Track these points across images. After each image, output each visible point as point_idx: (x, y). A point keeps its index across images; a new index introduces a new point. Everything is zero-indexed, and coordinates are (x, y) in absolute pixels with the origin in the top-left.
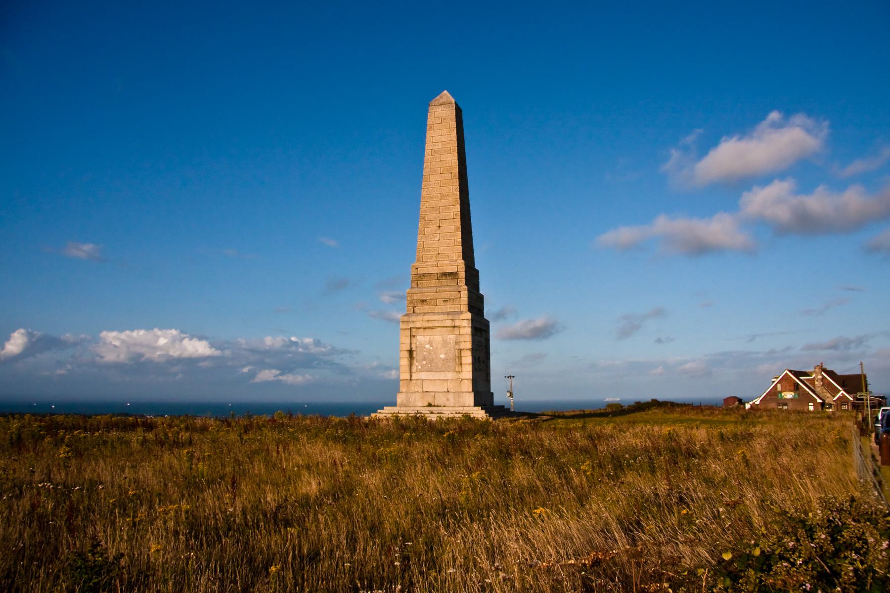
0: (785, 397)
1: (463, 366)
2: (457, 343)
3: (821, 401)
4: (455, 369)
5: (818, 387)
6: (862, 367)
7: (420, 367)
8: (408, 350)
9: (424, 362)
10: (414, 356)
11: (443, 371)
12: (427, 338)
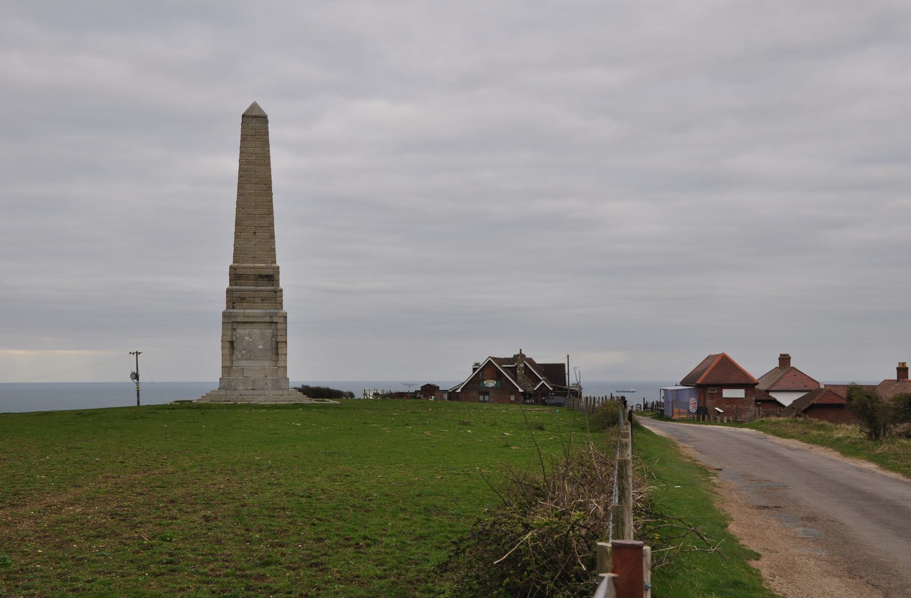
0: (487, 385)
1: (279, 355)
2: (273, 336)
3: (522, 391)
4: (272, 358)
5: (520, 376)
6: (568, 358)
7: (240, 356)
8: (229, 341)
9: (244, 352)
10: (235, 346)
11: (261, 360)
12: (247, 331)
